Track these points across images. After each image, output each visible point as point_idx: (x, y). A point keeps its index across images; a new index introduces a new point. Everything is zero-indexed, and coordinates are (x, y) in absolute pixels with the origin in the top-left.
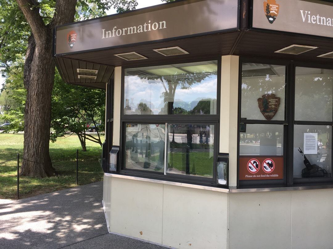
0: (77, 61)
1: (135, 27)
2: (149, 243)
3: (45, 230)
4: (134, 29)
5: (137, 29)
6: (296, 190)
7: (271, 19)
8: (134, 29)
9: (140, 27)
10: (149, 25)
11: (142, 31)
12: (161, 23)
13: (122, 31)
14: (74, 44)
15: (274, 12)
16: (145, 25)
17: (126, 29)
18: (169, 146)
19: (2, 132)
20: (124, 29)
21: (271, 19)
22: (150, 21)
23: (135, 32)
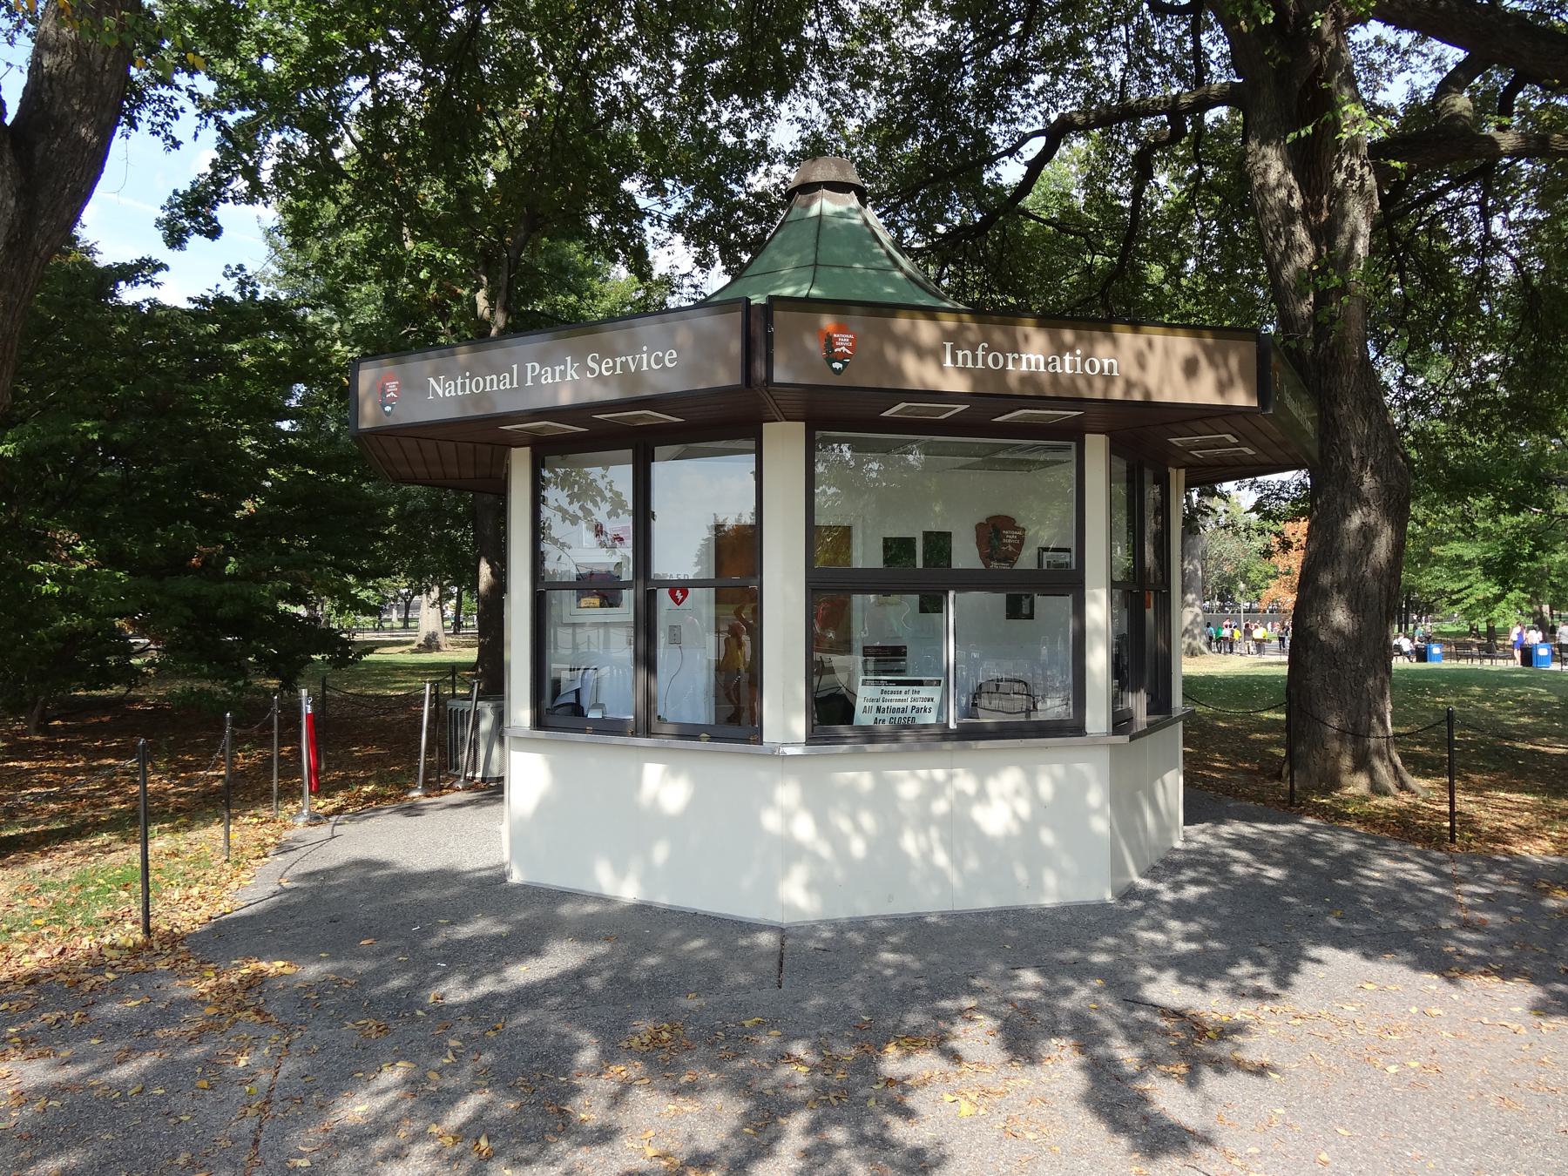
0: (489, 448)
1: (494, 377)
2: (650, 907)
3: (1254, 1049)
4: (492, 380)
5: (499, 381)
6: (966, 748)
7: (837, 365)
8: (492, 380)
9: (546, 372)
10: (645, 356)
11: (453, 394)
12: (488, 378)
13: (485, 381)
14: (392, 406)
15: (844, 349)
16: (459, 381)
17: (624, 359)
18: (888, 666)
19: (371, 651)
20: (557, 368)
21: (837, 365)
22: (645, 348)
23: (495, 388)
